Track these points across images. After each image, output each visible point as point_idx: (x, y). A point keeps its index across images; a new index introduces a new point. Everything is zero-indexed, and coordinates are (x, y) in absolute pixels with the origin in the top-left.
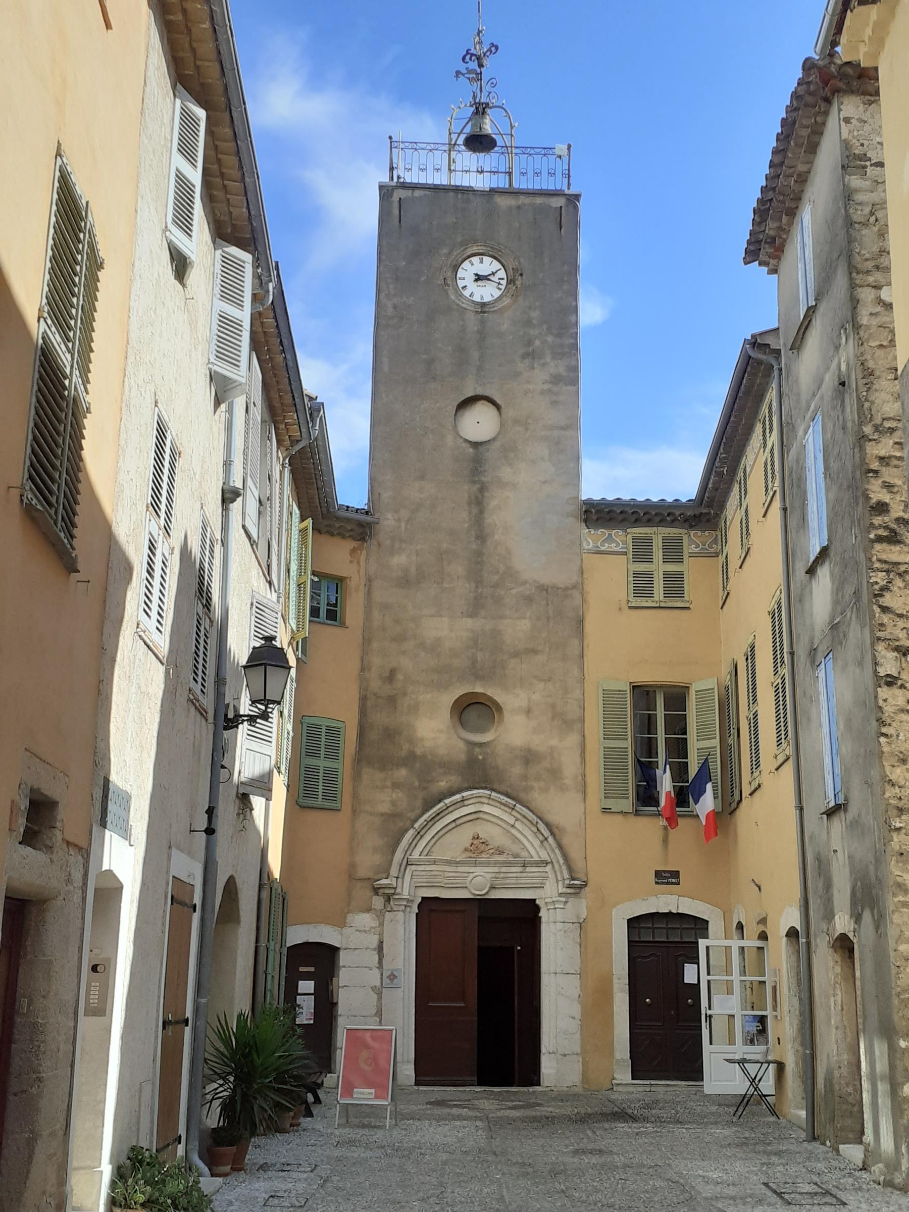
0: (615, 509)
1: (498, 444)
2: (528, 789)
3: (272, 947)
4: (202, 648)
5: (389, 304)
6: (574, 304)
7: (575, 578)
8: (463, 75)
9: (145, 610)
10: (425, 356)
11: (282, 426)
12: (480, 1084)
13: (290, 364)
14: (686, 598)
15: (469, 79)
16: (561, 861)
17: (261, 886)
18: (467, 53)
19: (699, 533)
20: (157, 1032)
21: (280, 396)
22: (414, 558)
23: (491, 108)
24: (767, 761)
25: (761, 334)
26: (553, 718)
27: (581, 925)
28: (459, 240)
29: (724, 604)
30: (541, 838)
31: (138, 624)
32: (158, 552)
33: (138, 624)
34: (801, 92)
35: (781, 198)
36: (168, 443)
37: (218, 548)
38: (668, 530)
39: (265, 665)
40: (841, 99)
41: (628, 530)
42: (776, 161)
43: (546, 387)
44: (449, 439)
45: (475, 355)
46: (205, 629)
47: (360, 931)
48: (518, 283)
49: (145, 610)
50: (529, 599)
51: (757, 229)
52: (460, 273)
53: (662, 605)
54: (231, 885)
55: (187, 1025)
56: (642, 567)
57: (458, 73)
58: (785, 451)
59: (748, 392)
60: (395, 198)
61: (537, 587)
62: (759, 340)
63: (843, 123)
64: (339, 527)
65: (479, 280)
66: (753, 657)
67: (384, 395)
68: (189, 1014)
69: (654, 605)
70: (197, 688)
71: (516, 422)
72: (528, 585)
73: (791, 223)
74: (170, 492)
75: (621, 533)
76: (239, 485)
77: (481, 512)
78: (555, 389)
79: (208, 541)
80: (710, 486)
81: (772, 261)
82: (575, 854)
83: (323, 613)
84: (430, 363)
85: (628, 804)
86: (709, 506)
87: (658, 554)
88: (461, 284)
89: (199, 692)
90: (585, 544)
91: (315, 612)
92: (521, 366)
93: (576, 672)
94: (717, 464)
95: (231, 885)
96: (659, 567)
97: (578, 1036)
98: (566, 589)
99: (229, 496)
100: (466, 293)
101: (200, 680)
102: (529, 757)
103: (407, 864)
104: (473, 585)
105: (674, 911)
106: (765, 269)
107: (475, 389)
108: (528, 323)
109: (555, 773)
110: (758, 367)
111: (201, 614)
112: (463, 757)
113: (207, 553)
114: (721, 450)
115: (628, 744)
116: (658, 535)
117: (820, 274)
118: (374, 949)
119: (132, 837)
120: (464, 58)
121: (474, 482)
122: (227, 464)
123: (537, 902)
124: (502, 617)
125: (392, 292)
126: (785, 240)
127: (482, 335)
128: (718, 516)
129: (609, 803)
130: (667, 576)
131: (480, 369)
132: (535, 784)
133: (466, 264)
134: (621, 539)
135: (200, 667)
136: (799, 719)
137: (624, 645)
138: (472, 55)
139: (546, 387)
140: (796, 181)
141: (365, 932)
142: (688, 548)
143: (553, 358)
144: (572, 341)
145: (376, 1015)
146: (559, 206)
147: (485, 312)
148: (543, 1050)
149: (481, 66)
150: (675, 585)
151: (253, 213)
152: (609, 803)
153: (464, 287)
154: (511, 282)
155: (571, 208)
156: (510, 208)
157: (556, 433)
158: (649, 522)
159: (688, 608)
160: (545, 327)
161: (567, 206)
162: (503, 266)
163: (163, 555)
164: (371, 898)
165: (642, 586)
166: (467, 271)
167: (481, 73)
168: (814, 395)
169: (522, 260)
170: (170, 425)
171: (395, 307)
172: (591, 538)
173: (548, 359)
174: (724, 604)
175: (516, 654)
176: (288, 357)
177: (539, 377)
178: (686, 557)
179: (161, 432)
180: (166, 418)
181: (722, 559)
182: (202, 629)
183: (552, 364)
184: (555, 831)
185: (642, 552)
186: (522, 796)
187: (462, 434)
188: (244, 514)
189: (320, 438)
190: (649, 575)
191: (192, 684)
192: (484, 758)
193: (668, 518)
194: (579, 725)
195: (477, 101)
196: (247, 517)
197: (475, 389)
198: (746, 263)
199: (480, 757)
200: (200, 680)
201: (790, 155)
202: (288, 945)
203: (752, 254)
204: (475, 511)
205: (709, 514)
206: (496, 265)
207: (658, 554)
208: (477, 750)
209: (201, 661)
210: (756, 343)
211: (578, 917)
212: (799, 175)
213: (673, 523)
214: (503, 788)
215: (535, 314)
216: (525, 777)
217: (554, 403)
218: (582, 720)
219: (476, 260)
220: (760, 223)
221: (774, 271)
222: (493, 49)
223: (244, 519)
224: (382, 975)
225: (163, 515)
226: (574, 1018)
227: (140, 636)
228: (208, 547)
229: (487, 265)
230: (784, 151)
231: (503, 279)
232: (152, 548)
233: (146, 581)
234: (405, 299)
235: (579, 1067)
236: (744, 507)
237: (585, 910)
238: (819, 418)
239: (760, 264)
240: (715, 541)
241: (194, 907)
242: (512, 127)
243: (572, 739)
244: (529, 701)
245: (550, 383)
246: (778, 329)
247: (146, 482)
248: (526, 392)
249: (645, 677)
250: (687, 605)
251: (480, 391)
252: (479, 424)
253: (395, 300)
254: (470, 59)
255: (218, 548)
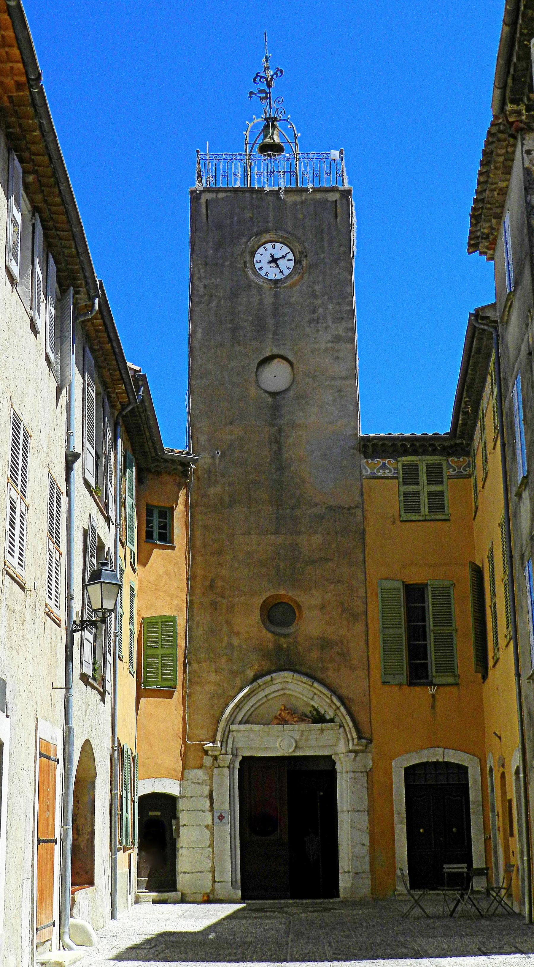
0: (387, 442)
1: (291, 393)
2: (324, 670)
3: (125, 795)
4: (54, 574)
5: (201, 285)
6: (349, 277)
7: (358, 499)
8: (255, 94)
9: (9, 552)
10: (231, 326)
11: (113, 395)
12: (292, 898)
13: (117, 350)
14: (447, 512)
15: (260, 97)
16: (351, 724)
17: (113, 750)
18: (258, 76)
19: (456, 459)
20: (33, 845)
21: (111, 374)
22: (227, 488)
23: (279, 121)
24: (502, 642)
25: (482, 309)
26: (343, 611)
27: (369, 773)
28: (255, 230)
29: (475, 516)
30: (334, 707)
31: (5, 563)
32: (18, 511)
33: (5, 563)
34: (495, 130)
35: (489, 206)
36: (22, 431)
37: (64, 500)
38: (432, 457)
39: (102, 583)
40: (524, 136)
41: (399, 459)
42: (482, 180)
43: (329, 345)
44: (253, 391)
45: (271, 322)
46: (56, 559)
47: (194, 783)
48: (304, 263)
49: (9, 552)
50: (321, 518)
51: (474, 229)
52: (257, 257)
53: (428, 518)
54: (87, 746)
55: (56, 844)
56: (411, 488)
57: (251, 93)
58: (503, 399)
59: (478, 351)
60: (203, 200)
61: (327, 507)
62: (480, 313)
63: (525, 155)
64: (165, 468)
65: (273, 260)
66: (492, 558)
67: (198, 358)
68: (57, 836)
69: (420, 518)
70: (52, 604)
71: (307, 375)
72: (319, 506)
73: (499, 223)
74: (24, 467)
75: (392, 461)
76: (79, 450)
77: (280, 449)
78: (337, 347)
79: (55, 495)
80: (460, 422)
81: (491, 252)
82: (362, 718)
83: (156, 535)
84: (234, 330)
85: (403, 678)
86: (461, 437)
87: (423, 478)
88: (258, 266)
89: (53, 606)
90: (364, 471)
91: (149, 536)
92: (308, 330)
93: (360, 576)
94: (463, 405)
95: (87, 746)
96: (424, 488)
97: (367, 859)
98: (350, 508)
99: (71, 459)
100: (262, 273)
101: (53, 597)
102: (324, 644)
103: (229, 731)
104: (275, 508)
105: (441, 760)
106: (484, 257)
107: (272, 350)
108: (314, 295)
109: (345, 656)
110: (483, 332)
111: (51, 549)
112: (271, 646)
113: (55, 504)
114: (465, 395)
115: (403, 631)
116: (422, 462)
117: (516, 268)
118: (206, 797)
119: (9, 706)
120: (255, 80)
121: (273, 425)
122: (69, 434)
123: (333, 757)
124: (299, 533)
125: (203, 275)
126: (496, 236)
127: (276, 306)
128: (469, 445)
129: (388, 678)
130: (430, 494)
131: (275, 333)
132: (330, 665)
133: (261, 250)
134: (393, 466)
135: (53, 588)
136: (516, 608)
137: (400, 550)
138: (262, 77)
139: (329, 345)
140: (498, 194)
141: (199, 783)
142: (447, 472)
143: (334, 322)
144: (348, 308)
145: (209, 846)
146: (334, 199)
147: (277, 288)
148: (341, 870)
149: (269, 86)
150: (437, 503)
151: (80, 251)
152: (388, 678)
153: (261, 269)
154: (298, 262)
155: (344, 201)
156: (295, 203)
157: (338, 383)
158: (415, 453)
159: (448, 520)
160: (326, 297)
161: (341, 199)
162: (291, 250)
163: (21, 511)
164: (202, 757)
165: (411, 504)
166: (262, 257)
167: (270, 93)
168: (517, 360)
169: (306, 244)
170: (22, 419)
171: (205, 287)
172: (371, 466)
173: (330, 323)
174: (475, 516)
175: (312, 562)
176: (115, 345)
177: (324, 340)
178: (445, 479)
179: (16, 422)
180: (20, 415)
181: (472, 480)
182: (53, 560)
183: (333, 327)
184: (346, 701)
185: (410, 475)
186: (319, 675)
187: (262, 386)
188: (84, 469)
189: (146, 398)
190: (417, 494)
191: (48, 601)
192: (288, 647)
193: (430, 449)
194: (364, 617)
195: (267, 117)
196: (87, 471)
197: (272, 350)
198: (470, 253)
199: (285, 646)
200: (53, 597)
201: (492, 176)
202: (139, 795)
203: (473, 247)
204: (275, 447)
205: (462, 443)
206: (286, 250)
207: (423, 478)
208: (282, 640)
209: (53, 583)
210: (478, 315)
211: (365, 767)
212: (501, 190)
213: (434, 452)
214: (304, 670)
215: (318, 288)
216: (321, 660)
217: (337, 358)
218: (366, 613)
219: (269, 246)
220: (476, 225)
221: (491, 259)
222: (279, 73)
223: (84, 473)
224: (213, 816)
225: (19, 483)
226: (364, 845)
227: (7, 572)
228: (55, 499)
229: (280, 250)
230: (487, 172)
231: (291, 260)
232: (13, 508)
233: (9, 532)
234: (213, 280)
235: (368, 882)
236: (483, 441)
237: (371, 762)
238: (519, 377)
239: (481, 253)
240: (468, 466)
241: (57, 761)
242: (296, 138)
243: (359, 628)
244: (323, 600)
245: (332, 342)
246: (495, 304)
247: (7, 462)
248: (313, 350)
249: (416, 577)
250: (447, 517)
251: (276, 351)
252: (276, 376)
253: (205, 282)
254: (260, 80)
255: (64, 500)
